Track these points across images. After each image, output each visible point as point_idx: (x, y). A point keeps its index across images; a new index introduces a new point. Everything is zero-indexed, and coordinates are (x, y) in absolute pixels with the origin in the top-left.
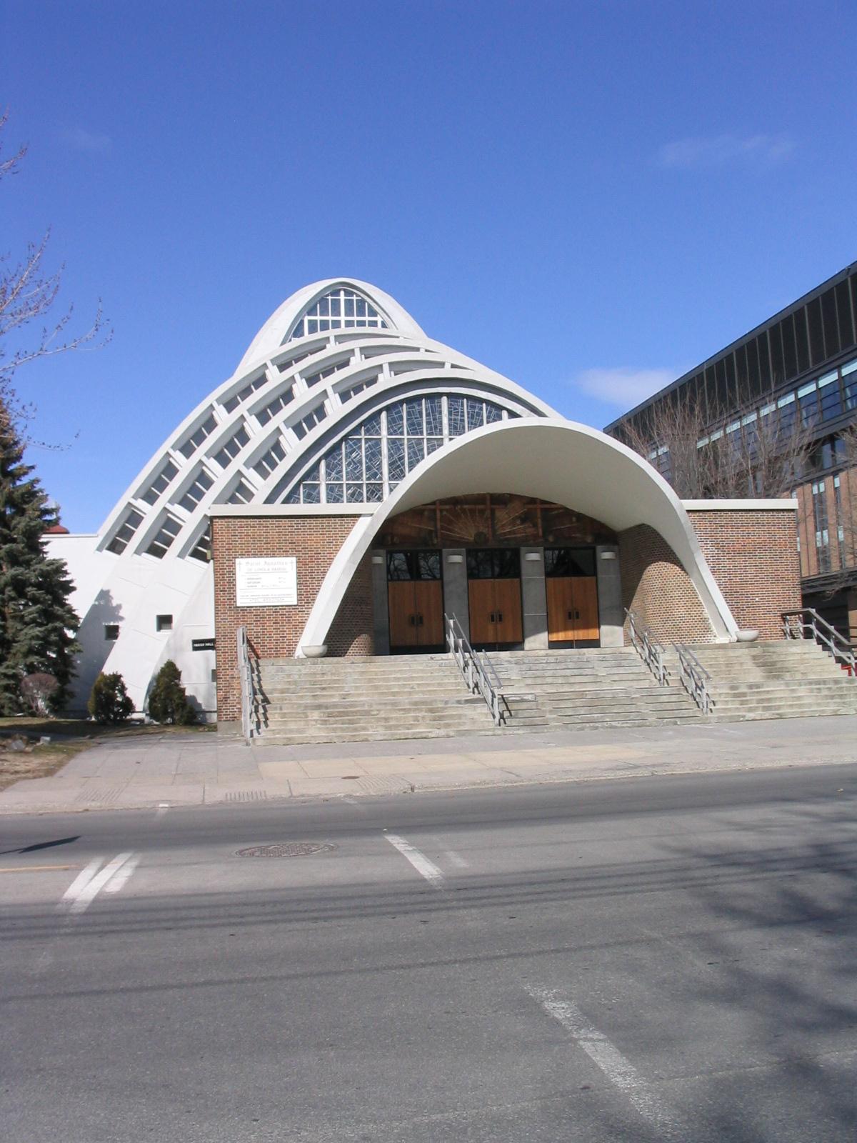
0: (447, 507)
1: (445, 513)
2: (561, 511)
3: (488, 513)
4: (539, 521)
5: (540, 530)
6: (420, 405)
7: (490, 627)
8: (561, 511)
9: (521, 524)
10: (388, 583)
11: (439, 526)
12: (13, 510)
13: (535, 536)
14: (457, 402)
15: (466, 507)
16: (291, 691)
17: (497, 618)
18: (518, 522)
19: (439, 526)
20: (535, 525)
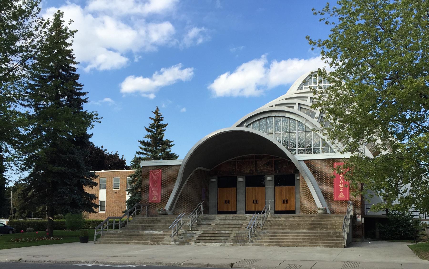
0: (240, 160)
1: (238, 163)
2: (282, 161)
3: (254, 162)
4: (274, 165)
5: (274, 168)
6: (273, 118)
7: (253, 205)
8: (282, 161)
9: (266, 166)
10: (246, 188)
11: (236, 168)
12: (357, 106)
13: (272, 171)
14: (279, 119)
15: (246, 160)
16: (309, 243)
17: (256, 202)
18: (265, 165)
19: (236, 168)
20: (272, 166)
